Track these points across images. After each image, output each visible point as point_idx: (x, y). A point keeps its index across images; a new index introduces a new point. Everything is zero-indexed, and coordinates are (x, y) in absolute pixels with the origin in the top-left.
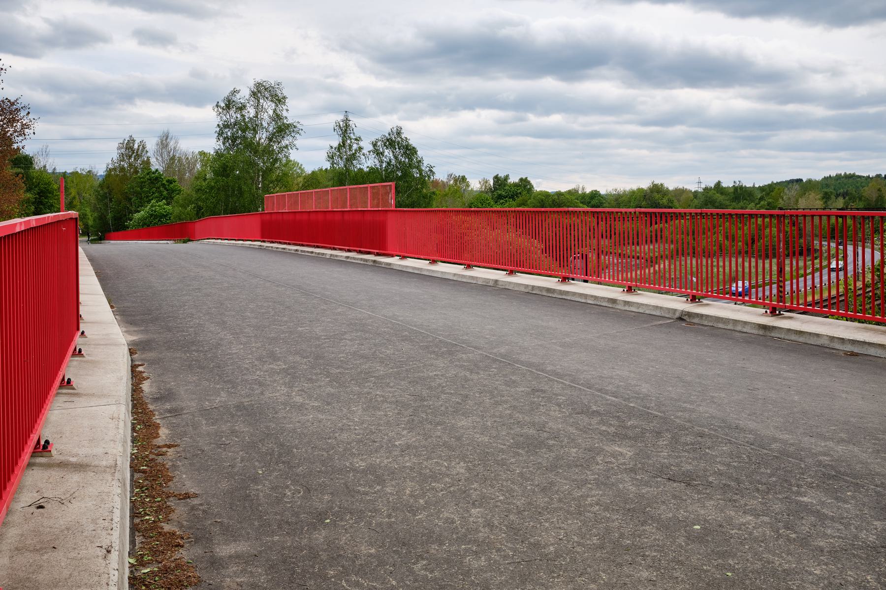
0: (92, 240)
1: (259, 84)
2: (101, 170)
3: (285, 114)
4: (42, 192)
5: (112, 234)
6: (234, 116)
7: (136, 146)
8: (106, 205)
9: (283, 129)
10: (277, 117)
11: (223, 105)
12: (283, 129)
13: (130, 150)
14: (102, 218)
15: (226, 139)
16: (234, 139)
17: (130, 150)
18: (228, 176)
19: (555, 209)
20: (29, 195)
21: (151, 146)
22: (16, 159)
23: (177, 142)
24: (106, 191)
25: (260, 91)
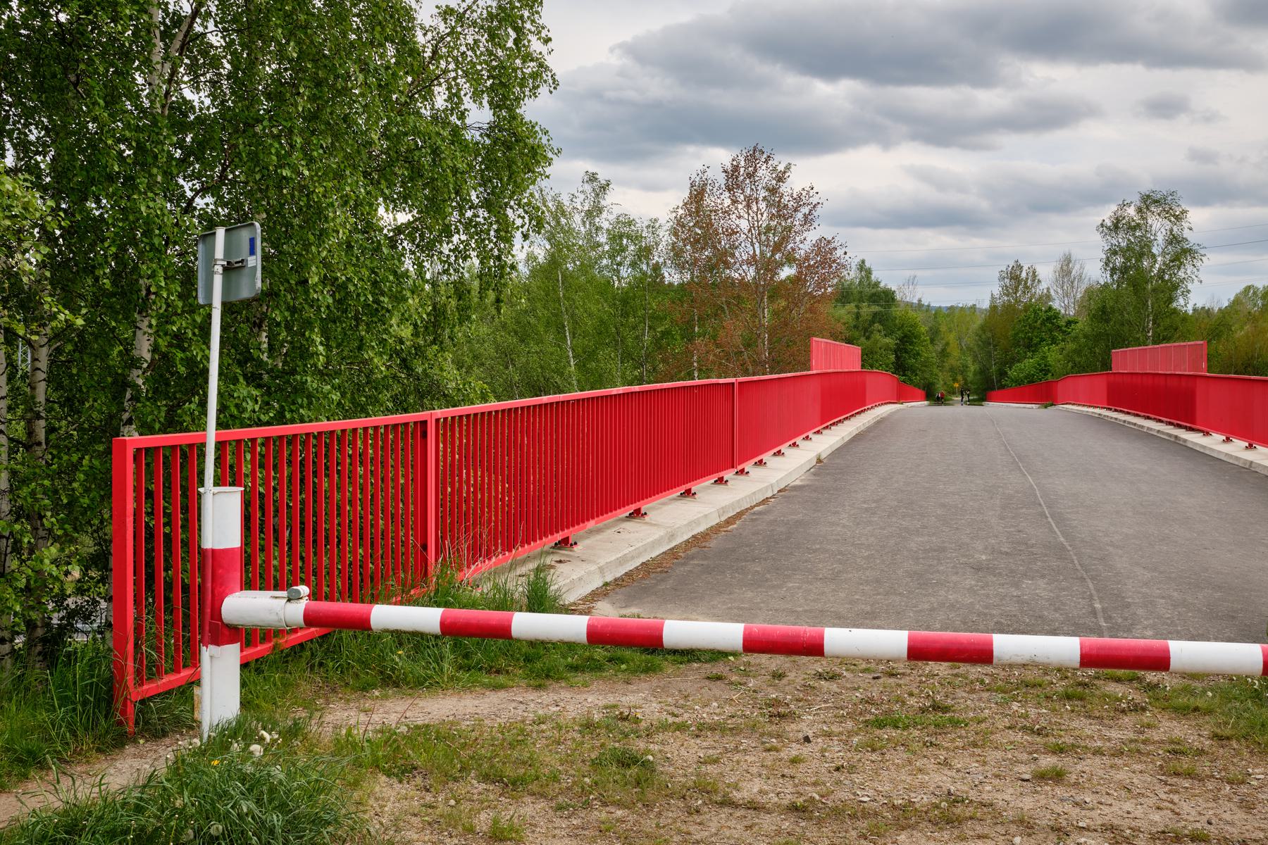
0: (974, 400)
1: (1148, 196)
2: (985, 305)
3: (1186, 234)
4: (906, 336)
5: (994, 393)
6: (1121, 240)
7: (1024, 275)
8: (989, 355)
9: (1181, 252)
10: (1174, 240)
11: (1109, 223)
12: (1181, 252)
13: (1016, 278)
14: (983, 371)
15: (1113, 271)
16: (1124, 270)
17: (1016, 278)
18: (1107, 321)
19: (130, 647)
20: (887, 340)
21: (1047, 274)
22: (874, 295)
23: (1082, 267)
24: (989, 335)
25: (1149, 201)
